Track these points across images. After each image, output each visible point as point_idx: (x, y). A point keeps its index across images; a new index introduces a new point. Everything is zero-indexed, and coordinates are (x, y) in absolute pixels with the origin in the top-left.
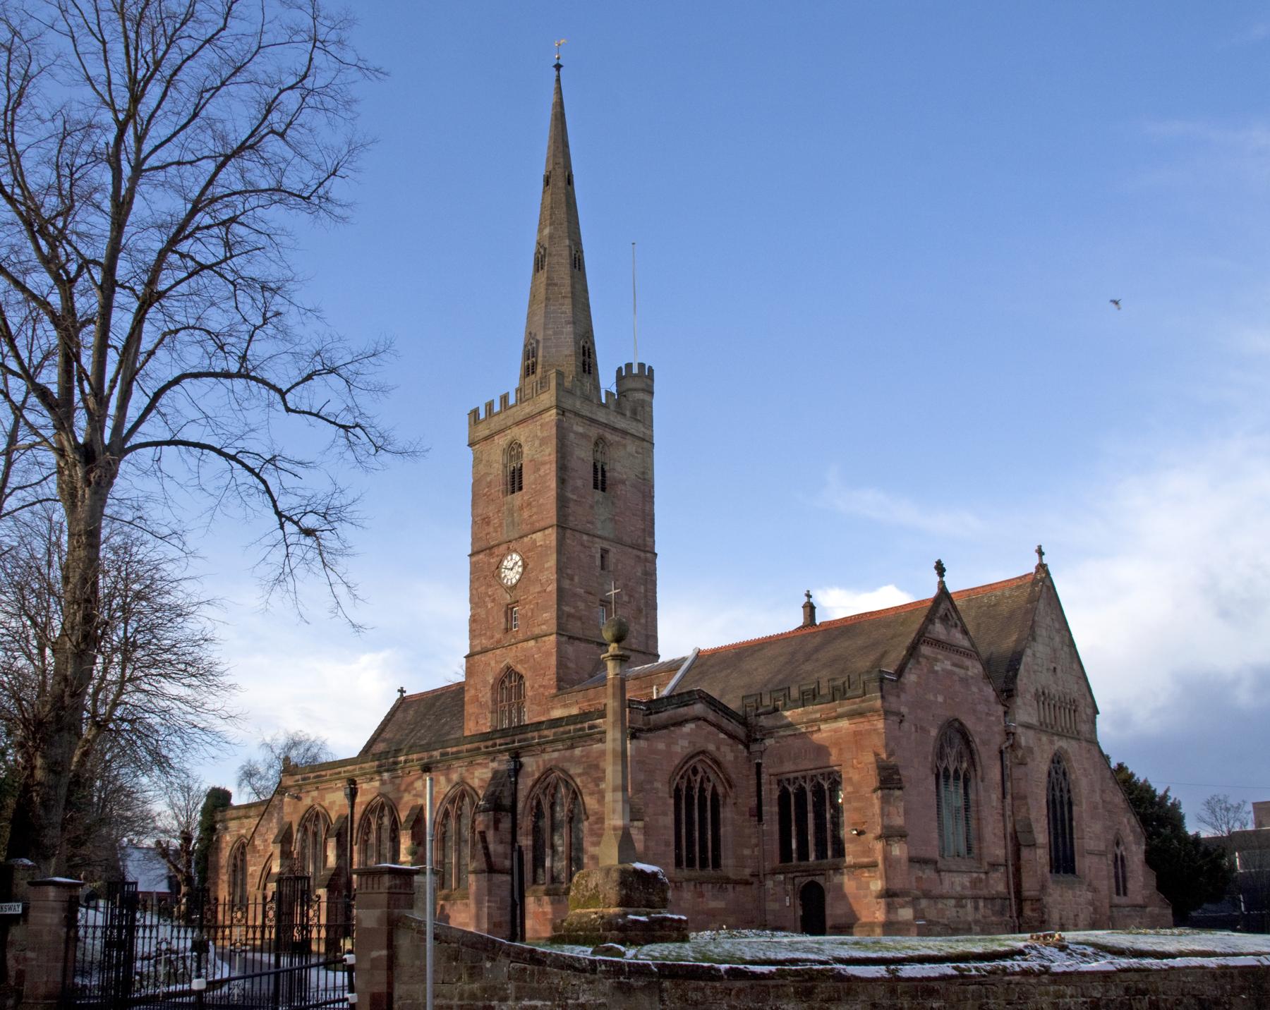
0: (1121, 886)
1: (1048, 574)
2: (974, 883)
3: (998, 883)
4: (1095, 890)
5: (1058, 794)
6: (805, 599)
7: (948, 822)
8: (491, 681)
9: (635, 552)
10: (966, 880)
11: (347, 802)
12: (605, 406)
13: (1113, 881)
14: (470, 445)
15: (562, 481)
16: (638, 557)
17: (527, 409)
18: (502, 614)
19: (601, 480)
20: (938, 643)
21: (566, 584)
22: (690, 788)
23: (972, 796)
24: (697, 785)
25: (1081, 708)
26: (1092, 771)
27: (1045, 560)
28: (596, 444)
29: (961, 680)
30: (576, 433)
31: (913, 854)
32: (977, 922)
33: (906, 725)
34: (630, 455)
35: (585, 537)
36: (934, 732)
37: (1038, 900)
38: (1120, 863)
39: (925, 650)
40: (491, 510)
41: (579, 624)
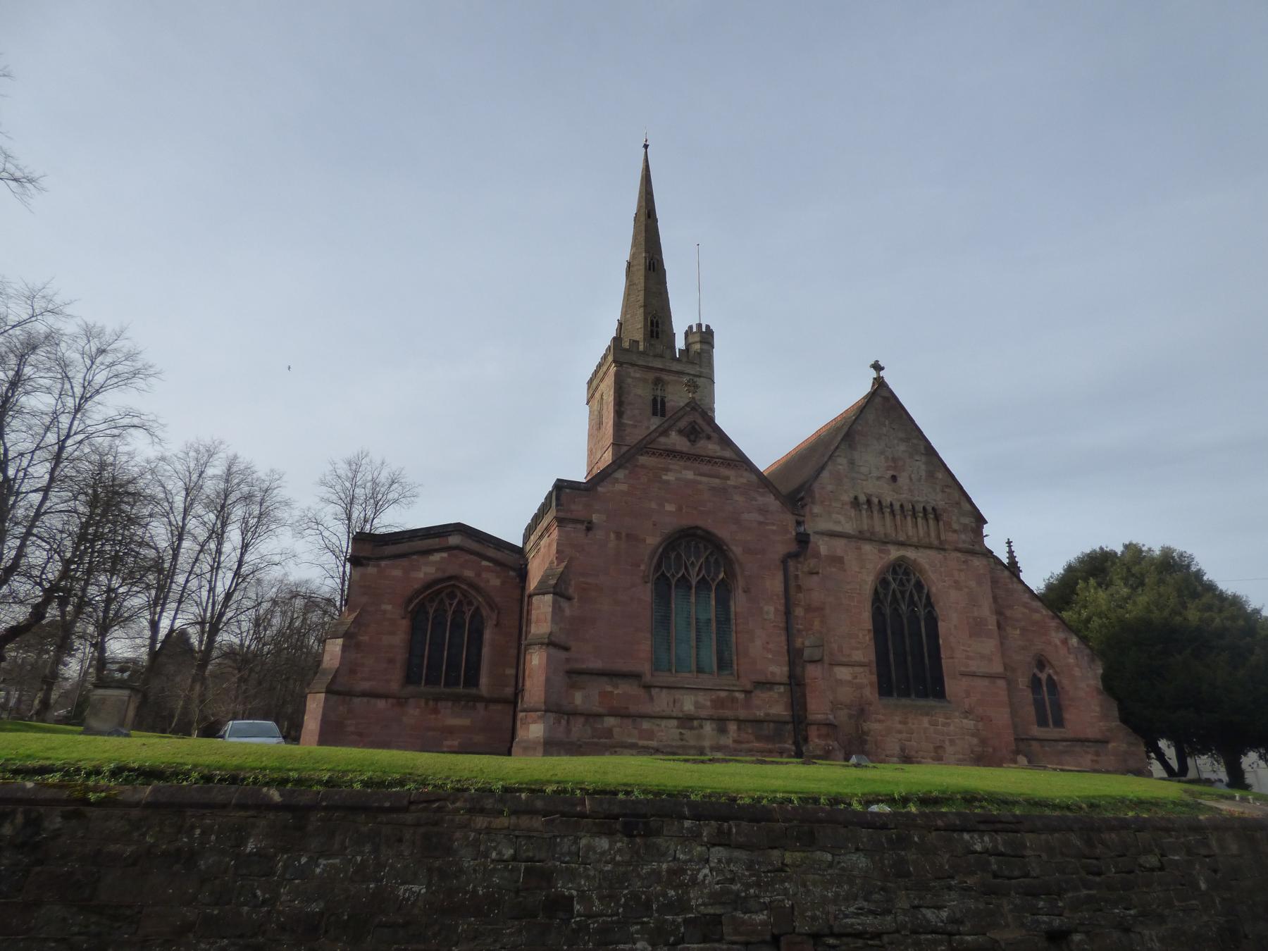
10: (703, 698)
12: (678, 360)
15: (619, 413)
33: (599, 534)
36: (653, 540)
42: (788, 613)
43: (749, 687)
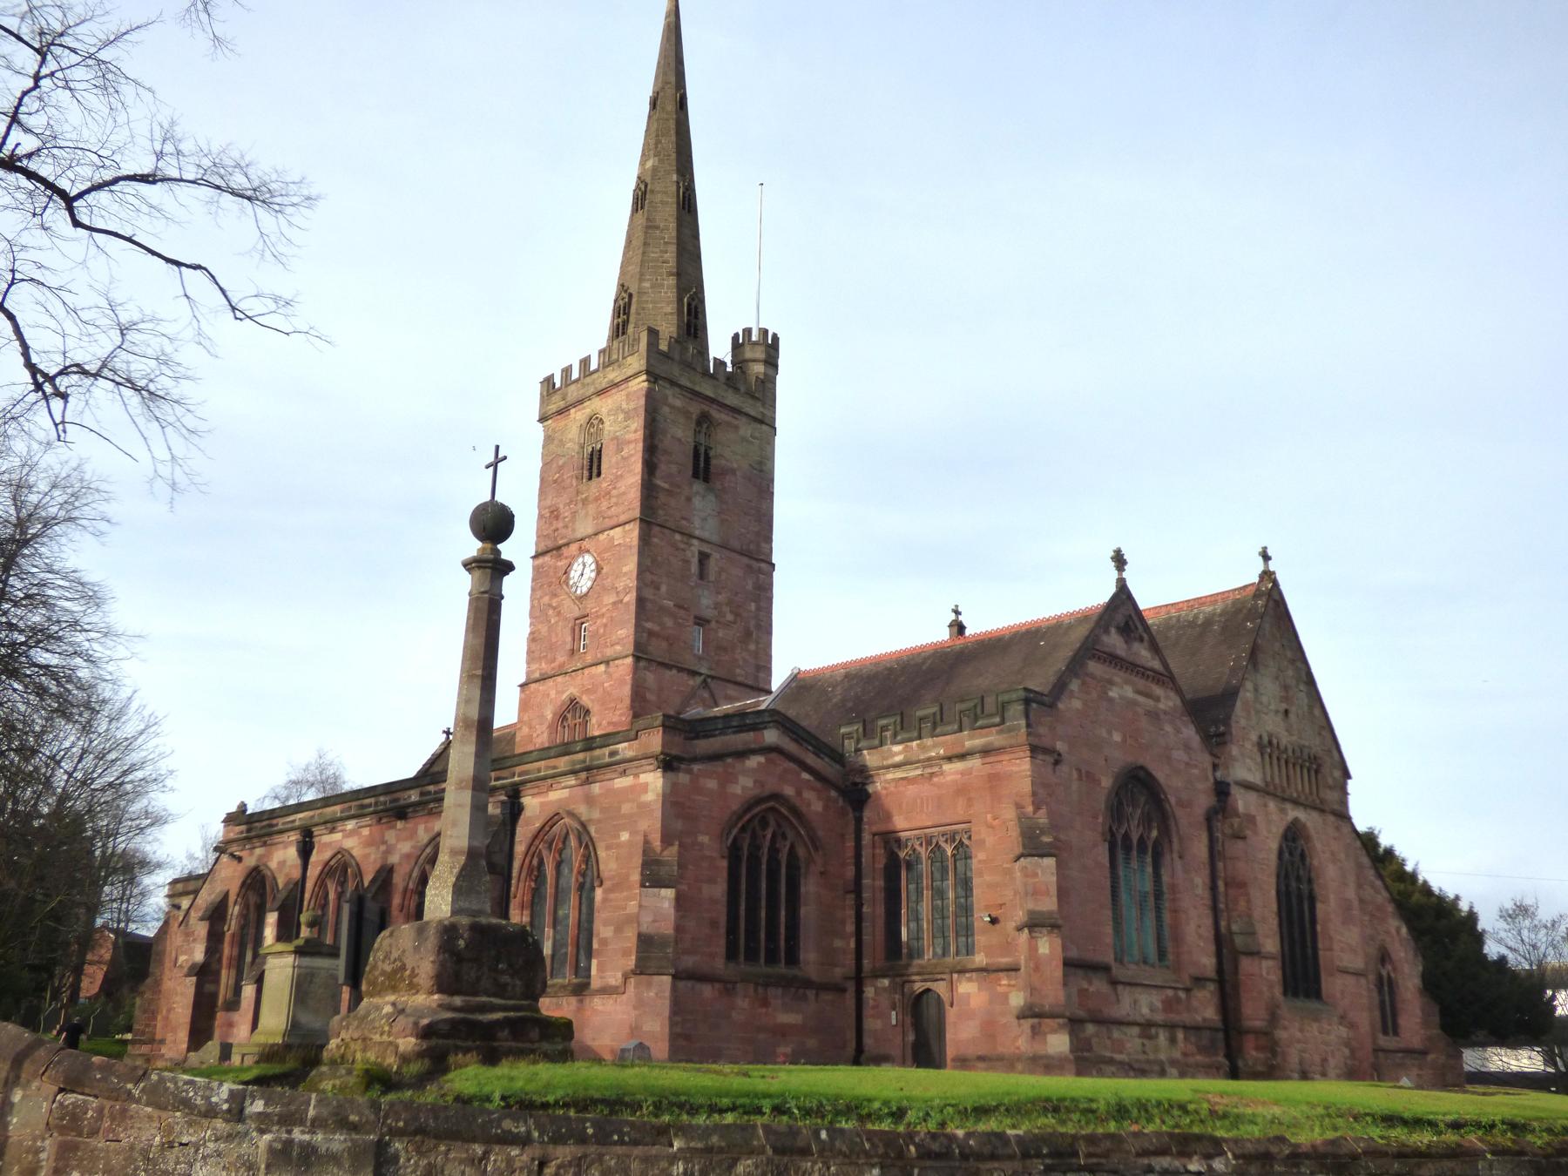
0: (1389, 1019)
1: (1275, 584)
2: (1169, 1005)
3: (1205, 1009)
4: (1352, 1026)
5: (1294, 884)
6: (953, 616)
7: (1130, 912)
8: (549, 716)
9: (745, 560)
10: (1156, 999)
11: (298, 862)
12: (712, 377)
13: (1377, 1013)
14: (542, 419)
15: (650, 467)
16: (749, 566)
17: (613, 375)
18: (568, 631)
19: (702, 468)
20: (1113, 659)
21: (649, 593)
22: (755, 847)
23: (1165, 878)
24: (767, 843)
25: (1325, 770)
26: (1342, 856)
27: (1272, 566)
28: (699, 423)
29: (1148, 713)
30: (672, 407)
31: (1074, 953)
32: (1173, 1063)
33: (1064, 769)
34: (744, 439)
35: (678, 537)
36: (1107, 782)
37: (1266, 1034)
38: (1386, 988)
39: (1093, 667)
40: (561, 502)
41: (664, 645)
42: (1213, 888)
43: (1188, 984)
